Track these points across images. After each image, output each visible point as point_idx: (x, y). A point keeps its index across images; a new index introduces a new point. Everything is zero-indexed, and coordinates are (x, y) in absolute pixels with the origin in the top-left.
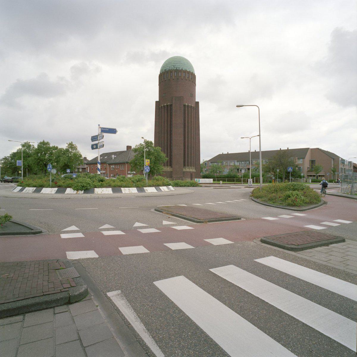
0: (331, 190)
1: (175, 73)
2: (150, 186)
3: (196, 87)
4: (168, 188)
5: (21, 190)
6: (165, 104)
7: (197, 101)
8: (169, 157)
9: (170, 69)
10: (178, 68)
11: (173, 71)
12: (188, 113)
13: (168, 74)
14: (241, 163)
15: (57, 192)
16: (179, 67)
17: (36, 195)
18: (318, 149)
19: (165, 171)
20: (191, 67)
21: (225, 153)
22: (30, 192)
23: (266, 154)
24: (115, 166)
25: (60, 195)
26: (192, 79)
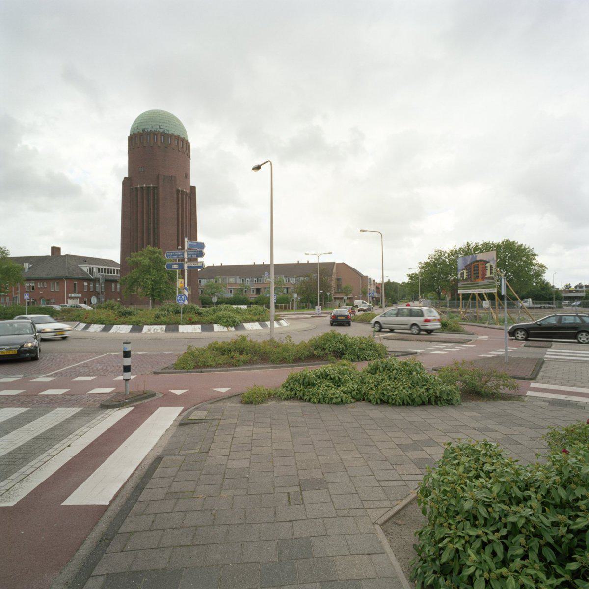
0: (531, 324)
1: (161, 138)
2: (253, 321)
3: (191, 161)
4: (280, 324)
5: (86, 328)
6: (145, 185)
7: (192, 184)
8: (486, 299)
9: (153, 130)
10: (166, 131)
11: (159, 135)
12: (182, 201)
13: (150, 137)
14: (246, 279)
15: (132, 331)
16: (168, 128)
17: (105, 334)
18: (343, 263)
21: (217, 264)
22: (99, 330)
23: (284, 269)
24: (36, 285)
25: (136, 335)
26: (182, 148)
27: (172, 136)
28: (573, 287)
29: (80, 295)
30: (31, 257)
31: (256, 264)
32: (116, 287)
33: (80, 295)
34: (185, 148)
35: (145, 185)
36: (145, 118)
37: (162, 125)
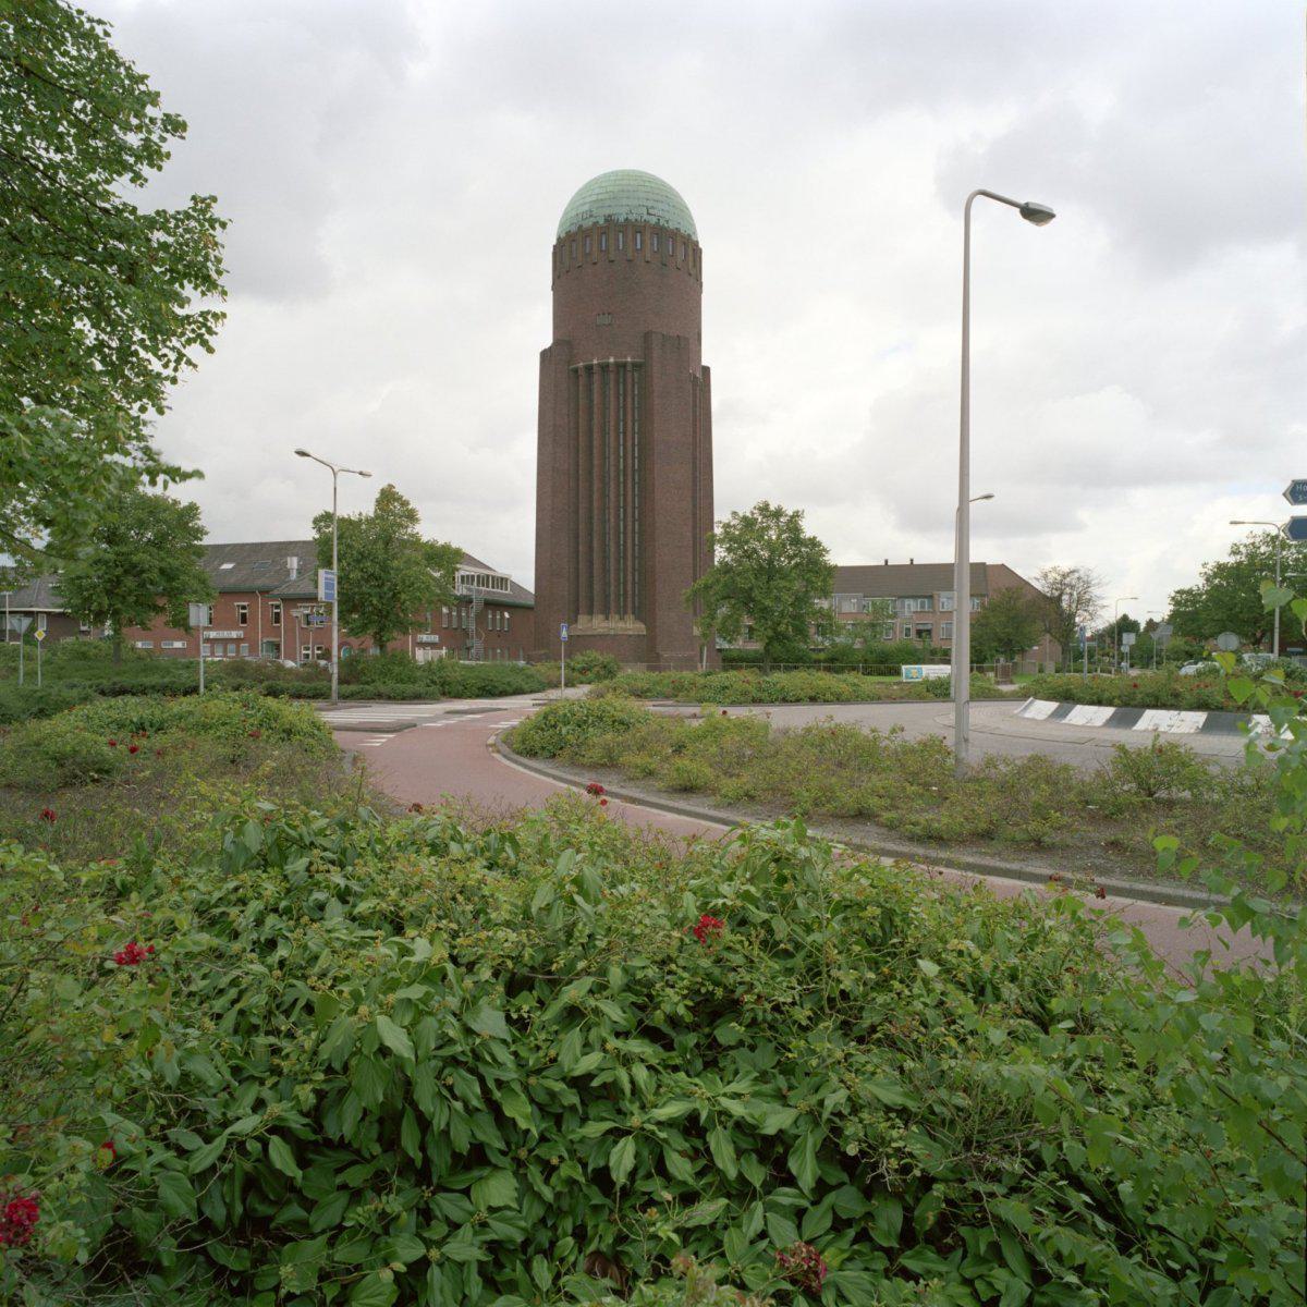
1: (652, 239)
6: (612, 360)
9: (632, 218)
19: (612, 632)
20: (682, 210)
28: (772, 508)
30: (291, 543)
35: (612, 360)
36: (611, 189)
37: (653, 207)
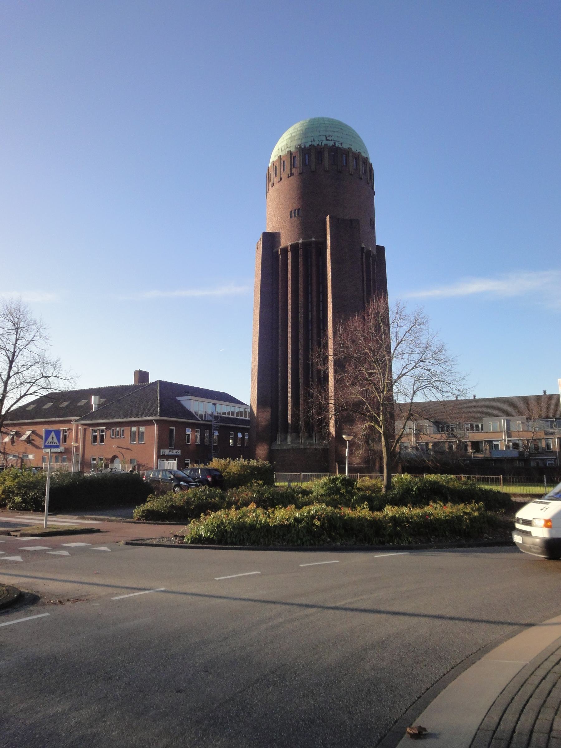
3: (375, 197)
9: (315, 144)
10: (337, 145)
16: (341, 140)
27: (348, 152)
29: (179, 452)
31: (477, 397)
32: (211, 435)
33: (179, 452)
34: (361, 171)
